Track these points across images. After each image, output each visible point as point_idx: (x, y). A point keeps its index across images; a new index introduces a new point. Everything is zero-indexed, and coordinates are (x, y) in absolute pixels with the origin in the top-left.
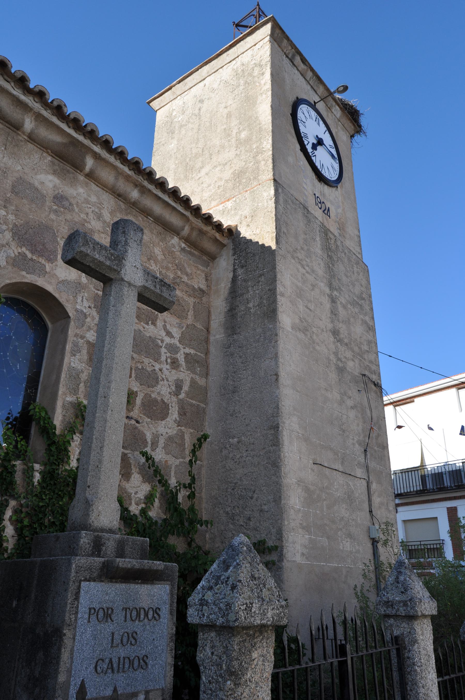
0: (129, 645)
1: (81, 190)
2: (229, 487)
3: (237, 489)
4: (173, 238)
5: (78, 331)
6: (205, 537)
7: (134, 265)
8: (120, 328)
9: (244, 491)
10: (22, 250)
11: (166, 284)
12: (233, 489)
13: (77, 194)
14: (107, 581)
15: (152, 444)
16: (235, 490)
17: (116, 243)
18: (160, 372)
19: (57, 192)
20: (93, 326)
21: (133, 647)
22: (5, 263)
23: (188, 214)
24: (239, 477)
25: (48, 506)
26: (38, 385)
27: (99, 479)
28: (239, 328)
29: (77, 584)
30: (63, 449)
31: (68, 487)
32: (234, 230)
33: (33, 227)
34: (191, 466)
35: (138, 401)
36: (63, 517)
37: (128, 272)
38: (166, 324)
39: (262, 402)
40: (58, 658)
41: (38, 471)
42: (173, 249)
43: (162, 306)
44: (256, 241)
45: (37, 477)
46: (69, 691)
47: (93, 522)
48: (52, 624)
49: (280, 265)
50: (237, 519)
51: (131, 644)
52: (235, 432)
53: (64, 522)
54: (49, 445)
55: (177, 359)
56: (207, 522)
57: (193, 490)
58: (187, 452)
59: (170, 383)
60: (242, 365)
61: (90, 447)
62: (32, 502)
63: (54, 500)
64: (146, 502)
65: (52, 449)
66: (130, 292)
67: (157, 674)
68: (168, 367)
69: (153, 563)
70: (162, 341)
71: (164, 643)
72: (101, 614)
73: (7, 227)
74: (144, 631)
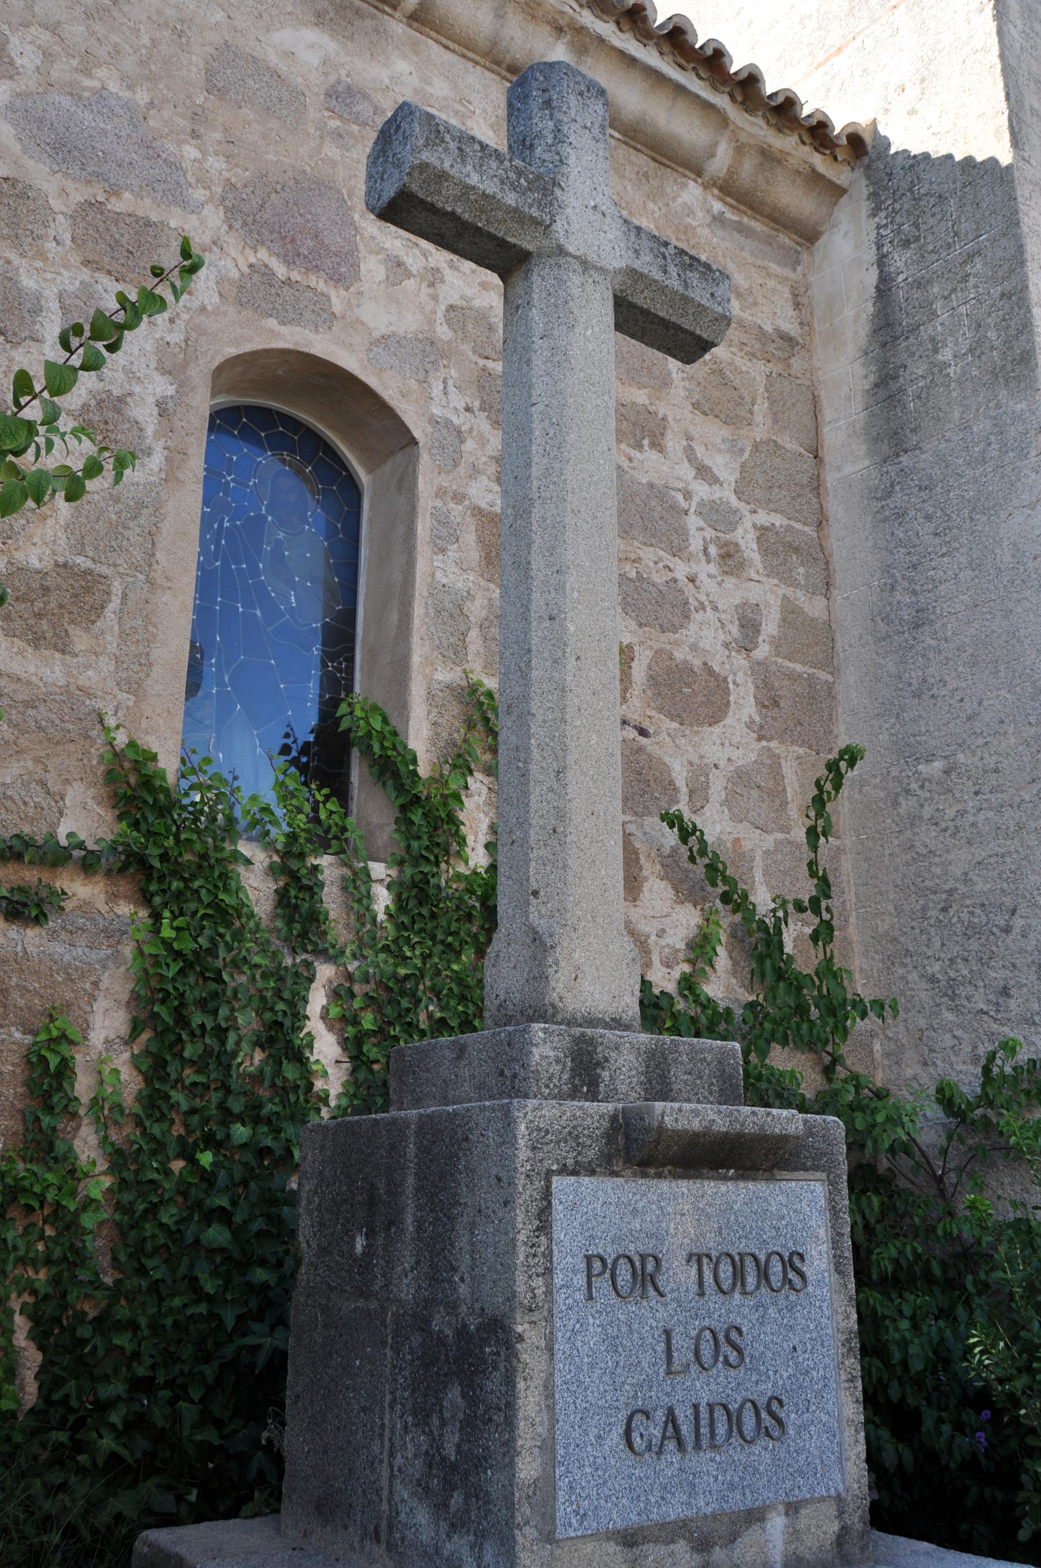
0: (720, 1365)
1: (402, 66)
2: (931, 905)
3: (955, 908)
4: (685, 186)
5: (444, 481)
6: (872, 1051)
7: (592, 204)
8: (571, 401)
9: (978, 911)
10: (259, 255)
11: (698, 260)
12: (944, 910)
13: (391, 78)
14: (629, 1172)
15: (691, 793)
16: (951, 912)
17: (528, 143)
18: (691, 585)
19: (332, 78)
20: (485, 463)
21: (732, 1372)
22: (216, 299)
23: (721, 101)
24: (959, 873)
25: (422, 977)
26: (352, 649)
27: (565, 867)
28: (914, 431)
29: (539, 1184)
30: (443, 816)
31: (470, 922)
32: (868, 138)
33: (279, 187)
34: (814, 848)
35: (639, 672)
36: (467, 1007)
37: (574, 227)
38: (694, 444)
39: (1014, 641)
40: (509, 1407)
41: (382, 880)
42: (689, 220)
43: (692, 334)
44: (943, 152)
45: (382, 899)
46: (553, 1507)
47: (561, 998)
48: (478, 1306)
49: (1032, 214)
50: (964, 994)
51: (727, 1362)
52: (933, 742)
53: (471, 1018)
54: (403, 808)
55: (737, 545)
56: (879, 1005)
57: (826, 916)
58: (793, 811)
59: (723, 616)
60: (937, 541)
61: (524, 775)
62: (378, 966)
63: (437, 960)
64: (692, 956)
65: (413, 818)
66: (589, 288)
67: (816, 1453)
68: (712, 568)
69: (768, 1114)
70: (687, 495)
71: (827, 1361)
72: (624, 1273)
73: (207, 193)
74: (762, 1324)
